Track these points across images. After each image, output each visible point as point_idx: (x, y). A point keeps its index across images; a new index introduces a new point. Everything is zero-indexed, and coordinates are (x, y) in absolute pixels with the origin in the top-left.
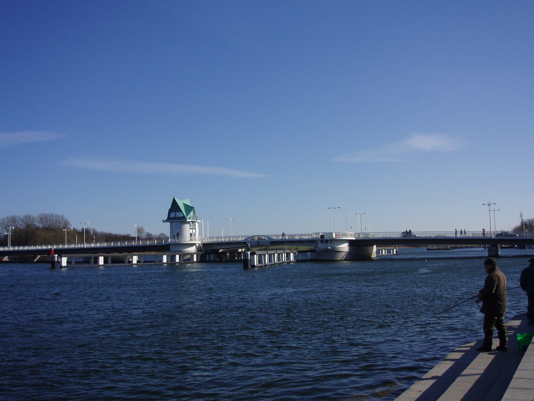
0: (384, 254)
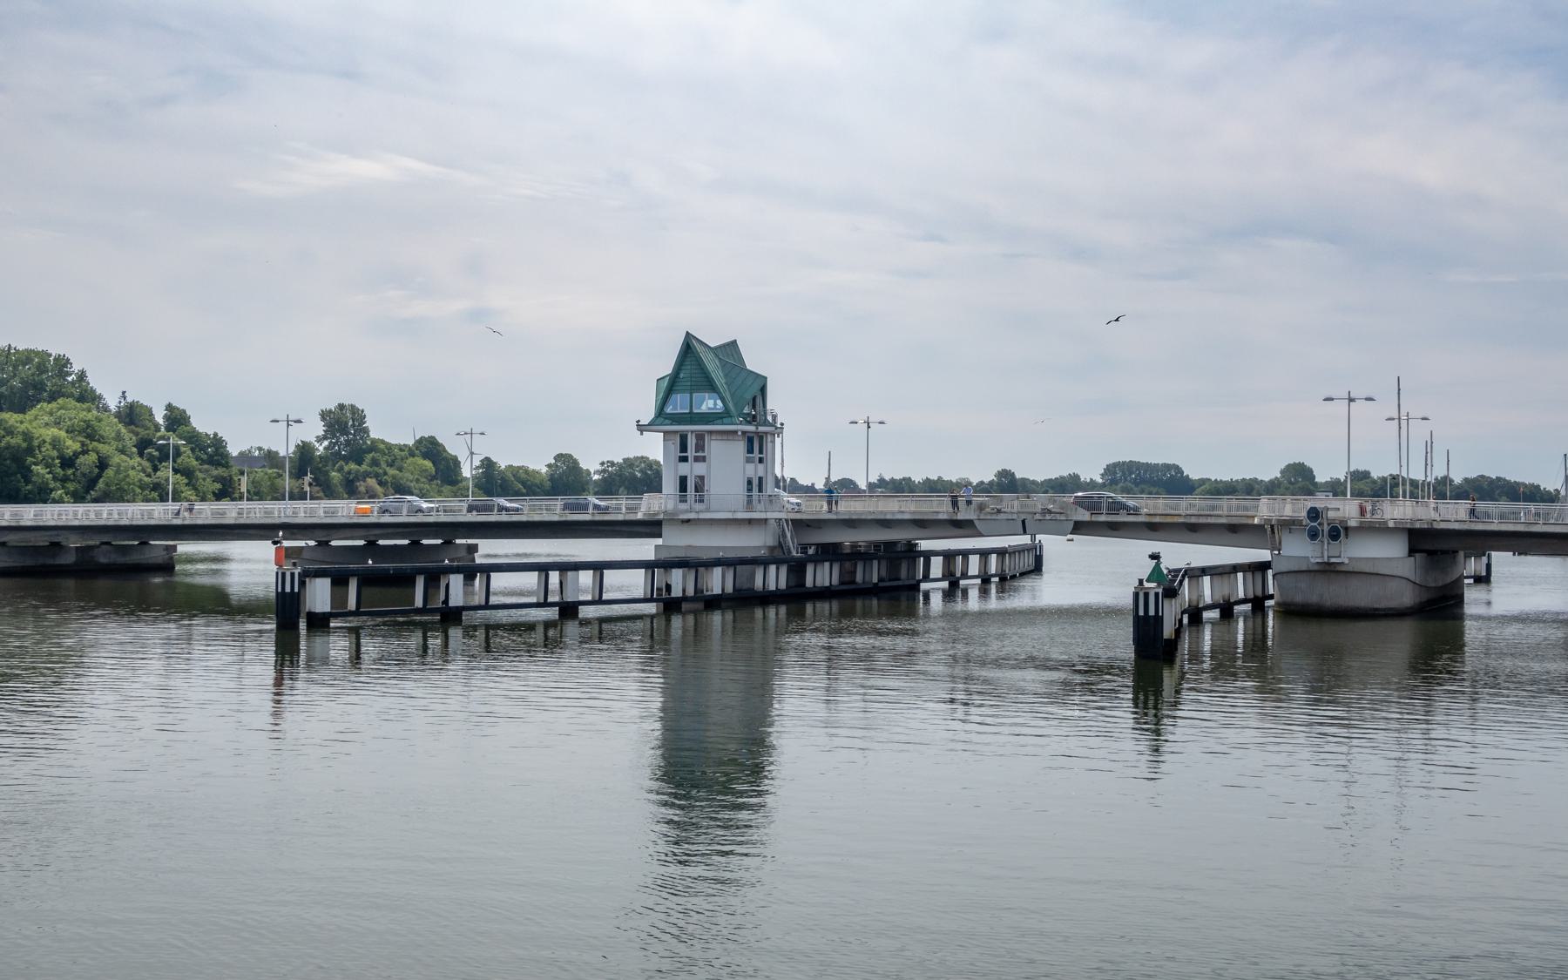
0: (288, 589)
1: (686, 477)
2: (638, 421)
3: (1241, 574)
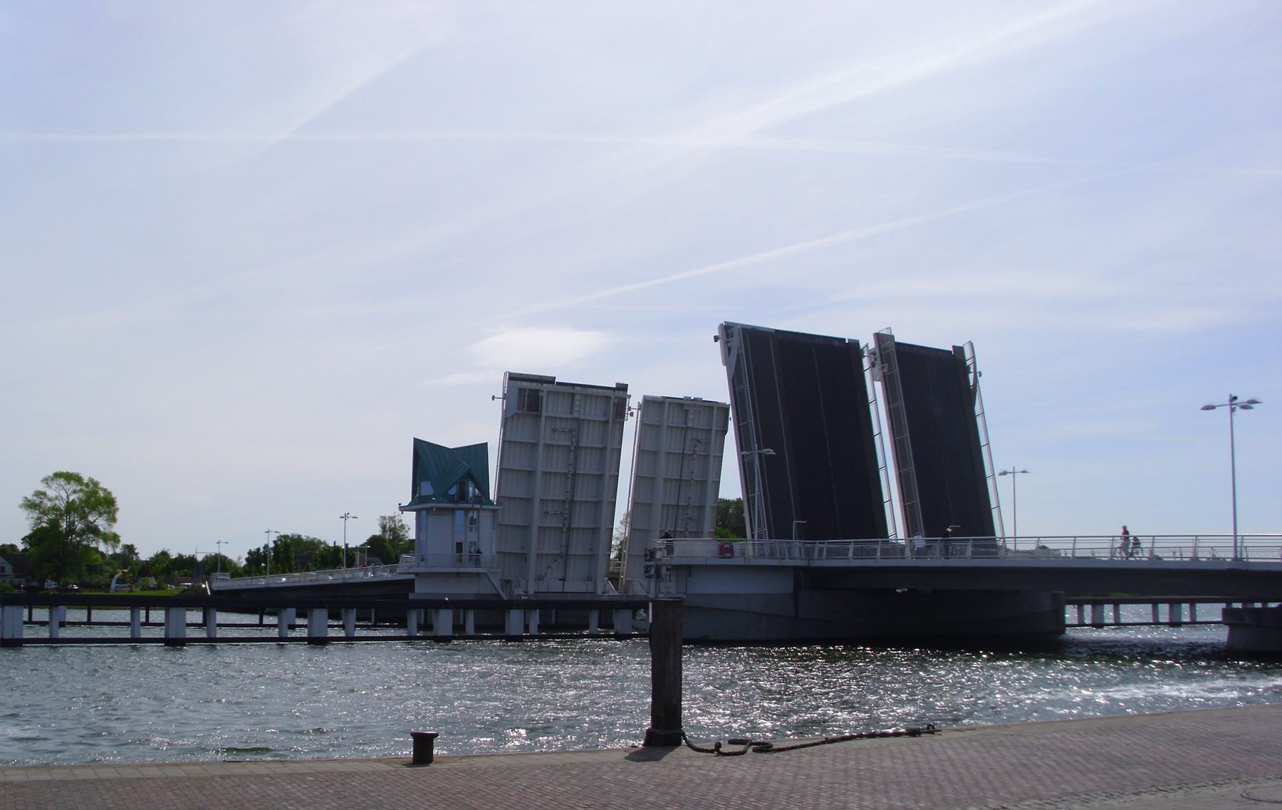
1: (462, 543)
2: (400, 504)
3: (1188, 605)
